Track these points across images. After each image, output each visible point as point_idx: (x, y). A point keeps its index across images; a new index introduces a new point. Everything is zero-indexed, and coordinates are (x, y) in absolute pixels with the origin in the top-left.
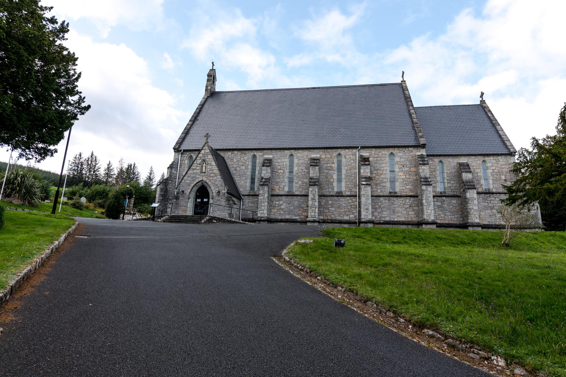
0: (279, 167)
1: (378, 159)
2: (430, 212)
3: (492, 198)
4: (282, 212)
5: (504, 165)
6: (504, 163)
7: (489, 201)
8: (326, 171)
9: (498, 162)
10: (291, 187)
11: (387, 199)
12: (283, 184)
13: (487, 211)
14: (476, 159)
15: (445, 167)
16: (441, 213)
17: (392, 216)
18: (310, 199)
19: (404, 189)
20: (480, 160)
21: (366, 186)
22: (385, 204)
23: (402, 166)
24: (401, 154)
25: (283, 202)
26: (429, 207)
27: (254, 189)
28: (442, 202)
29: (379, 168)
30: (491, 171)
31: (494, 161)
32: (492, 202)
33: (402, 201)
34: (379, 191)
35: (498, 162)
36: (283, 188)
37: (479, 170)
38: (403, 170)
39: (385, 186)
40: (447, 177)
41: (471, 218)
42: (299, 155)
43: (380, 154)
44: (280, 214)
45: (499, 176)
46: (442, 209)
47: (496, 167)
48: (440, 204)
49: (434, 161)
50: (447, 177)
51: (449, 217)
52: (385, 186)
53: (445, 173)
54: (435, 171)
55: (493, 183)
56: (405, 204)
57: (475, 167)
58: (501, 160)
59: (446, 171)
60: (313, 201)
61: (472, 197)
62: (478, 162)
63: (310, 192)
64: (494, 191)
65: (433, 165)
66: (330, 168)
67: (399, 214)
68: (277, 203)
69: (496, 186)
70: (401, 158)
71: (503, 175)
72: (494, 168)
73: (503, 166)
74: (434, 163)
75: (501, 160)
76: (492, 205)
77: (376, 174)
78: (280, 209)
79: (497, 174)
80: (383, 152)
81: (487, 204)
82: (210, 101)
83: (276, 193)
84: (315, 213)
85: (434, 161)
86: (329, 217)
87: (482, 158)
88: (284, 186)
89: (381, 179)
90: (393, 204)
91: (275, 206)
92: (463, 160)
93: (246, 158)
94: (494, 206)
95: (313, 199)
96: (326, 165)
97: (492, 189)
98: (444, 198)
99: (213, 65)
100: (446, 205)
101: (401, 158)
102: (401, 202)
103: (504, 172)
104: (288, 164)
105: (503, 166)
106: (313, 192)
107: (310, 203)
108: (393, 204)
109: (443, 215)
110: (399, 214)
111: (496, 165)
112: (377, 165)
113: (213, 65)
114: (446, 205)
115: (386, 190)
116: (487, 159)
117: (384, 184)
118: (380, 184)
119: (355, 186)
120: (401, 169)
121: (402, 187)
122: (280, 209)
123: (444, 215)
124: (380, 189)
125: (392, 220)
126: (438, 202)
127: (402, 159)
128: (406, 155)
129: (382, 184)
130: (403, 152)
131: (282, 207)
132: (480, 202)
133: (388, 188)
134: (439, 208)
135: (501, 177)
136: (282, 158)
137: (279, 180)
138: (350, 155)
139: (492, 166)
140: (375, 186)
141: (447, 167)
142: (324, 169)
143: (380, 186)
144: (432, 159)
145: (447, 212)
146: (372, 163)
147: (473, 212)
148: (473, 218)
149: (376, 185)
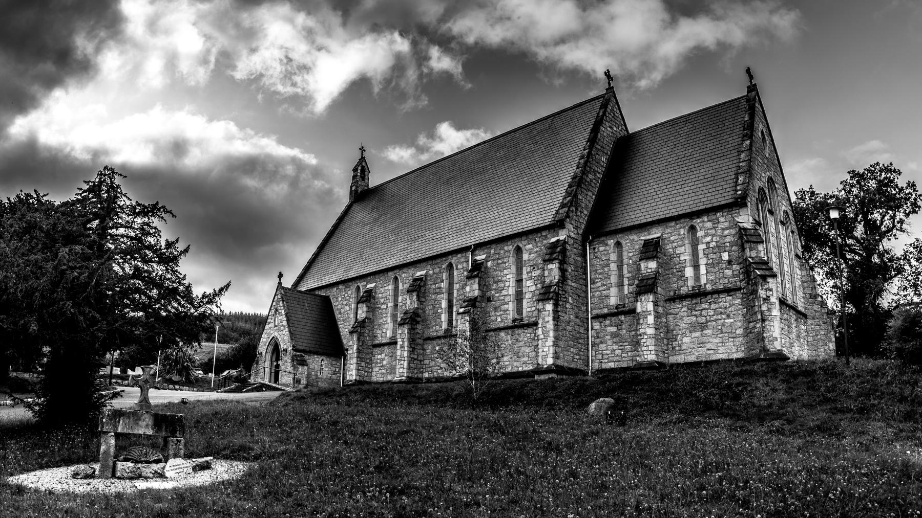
0: (382, 301)
1: (499, 261)
2: (547, 350)
3: (704, 306)
4: (384, 371)
5: (726, 229)
6: (726, 224)
7: (698, 313)
8: (433, 297)
9: (716, 225)
10: (519, 310)
11: (510, 332)
12: (386, 326)
13: (694, 335)
14: (678, 226)
15: (625, 254)
16: (615, 347)
17: (515, 364)
18: (398, 347)
19: (533, 311)
20: (684, 227)
21: (464, 315)
22: (506, 343)
23: (532, 268)
24: (530, 246)
25: (386, 355)
26: (546, 341)
27: (522, 314)
28: (619, 326)
29: (500, 278)
30: (704, 246)
31: (709, 225)
32: (704, 313)
33: (531, 333)
34: (499, 319)
35: (716, 225)
36: (386, 333)
37: (682, 249)
38: (534, 275)
39: (507, 310)
40: (629, 272)
41: (641, 353)
42: (403, 275)
43: (502, 252)
44: (382, 374)
45: (718, 255)
46: (617, 339)
47: (713, 235)
48: (614, 329)
49: (607, 245)
50: (629, 272)
51: (629, 354)
52: (507, 310)
53: (625, 266)
54: (608, 265)
55: (707, 272)
56: (534, 340)
57: (675, 244)
58: (722, 219)
59: (625, 261)
60: (402, 349)
61: (644, 309)
62: (682, 231)
63: (398, 336)
64: (709, 287)
65: (605, 252)
66: (438, 290)
67: (526, 359)
68: (379, 357)
69: (712, 278)
70: (530, 254)
71: (725, 251)
72: (708, 239)
73: (726, 232)
74: (607, 248)
75: (722, 219)
76: (703, 320)
77: (495, 289)
78: (382, 367)
79: (715, 251)
80: (506, 248)
81: (694, 319)
82: (356, 207)
83: (378, 342)
84: (404, 368)
85: (607, 245)
86: (435, 373)
87: (687, 223)
88: (387, 330)
89: (502, 298)
90: (517, 340)
91: (377, 363)
92: (655, 234)
93: (349, 292)
94: (707, 321)
95: (402, 347)
96: (433, 287)
97: (705, 284)
98: (623, 318)
99: (751, 77)
100: (625, 331)
101: (530, 254)
102: (529, 335)
103: (728, 244)
104: (391, 293)
105: (726, 232)
106: (402, 335)
107: (399, 353)
108: (517, 340)
109: (618, 352)
110: (526, 359)
111: (713, 231)
112: (497, 272)
113: (751, 77)
114: (625, 331)
115: (509, 318)
116: (697, 222)
117: (505, 306)
118: (499, 307)
119: (265, 345)
120: (530, 274)
121: (531, 307)
122: (382, 367)
123: (620, 351)
124: (501, 315)
125: (515, 370)
126: (612, 326)
127: (532, 255)
128: (537, 247)
129: (503, 307)
130: (533, 241)
131: (385, 362)
132: (683, 317)
133: (511, 313)
134: (614, 338)
135: (721, 257)
136: (385, 285)
137: (381, 321)
138: (463, 262)
139: (707, 235)
140: (493, 313)
141: (629, 252)
142: (432, 294)
143: (500, 311)
144: (603, 241)
145: (626, 344)
146: (491, 271)
147: (644, 340)
148: (645, 353)
149: (496, 309)
